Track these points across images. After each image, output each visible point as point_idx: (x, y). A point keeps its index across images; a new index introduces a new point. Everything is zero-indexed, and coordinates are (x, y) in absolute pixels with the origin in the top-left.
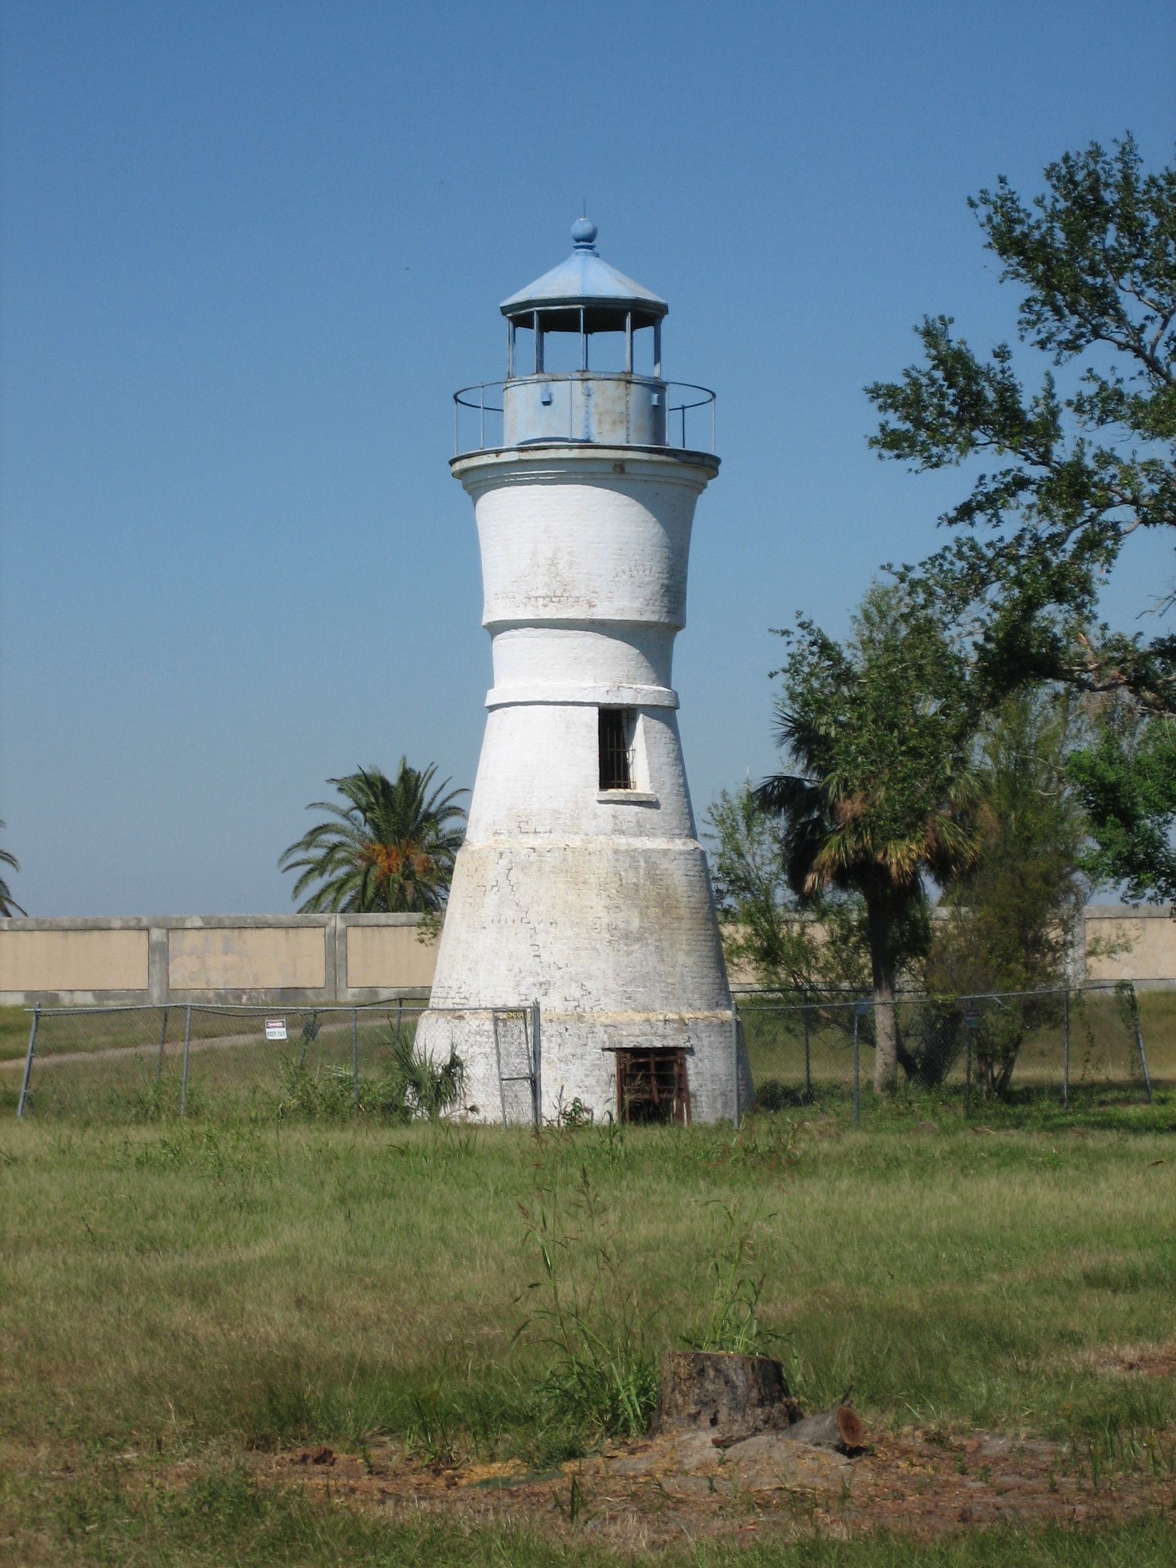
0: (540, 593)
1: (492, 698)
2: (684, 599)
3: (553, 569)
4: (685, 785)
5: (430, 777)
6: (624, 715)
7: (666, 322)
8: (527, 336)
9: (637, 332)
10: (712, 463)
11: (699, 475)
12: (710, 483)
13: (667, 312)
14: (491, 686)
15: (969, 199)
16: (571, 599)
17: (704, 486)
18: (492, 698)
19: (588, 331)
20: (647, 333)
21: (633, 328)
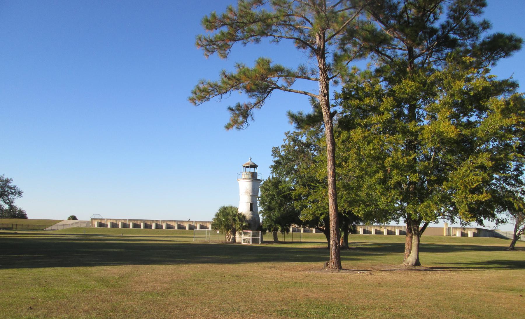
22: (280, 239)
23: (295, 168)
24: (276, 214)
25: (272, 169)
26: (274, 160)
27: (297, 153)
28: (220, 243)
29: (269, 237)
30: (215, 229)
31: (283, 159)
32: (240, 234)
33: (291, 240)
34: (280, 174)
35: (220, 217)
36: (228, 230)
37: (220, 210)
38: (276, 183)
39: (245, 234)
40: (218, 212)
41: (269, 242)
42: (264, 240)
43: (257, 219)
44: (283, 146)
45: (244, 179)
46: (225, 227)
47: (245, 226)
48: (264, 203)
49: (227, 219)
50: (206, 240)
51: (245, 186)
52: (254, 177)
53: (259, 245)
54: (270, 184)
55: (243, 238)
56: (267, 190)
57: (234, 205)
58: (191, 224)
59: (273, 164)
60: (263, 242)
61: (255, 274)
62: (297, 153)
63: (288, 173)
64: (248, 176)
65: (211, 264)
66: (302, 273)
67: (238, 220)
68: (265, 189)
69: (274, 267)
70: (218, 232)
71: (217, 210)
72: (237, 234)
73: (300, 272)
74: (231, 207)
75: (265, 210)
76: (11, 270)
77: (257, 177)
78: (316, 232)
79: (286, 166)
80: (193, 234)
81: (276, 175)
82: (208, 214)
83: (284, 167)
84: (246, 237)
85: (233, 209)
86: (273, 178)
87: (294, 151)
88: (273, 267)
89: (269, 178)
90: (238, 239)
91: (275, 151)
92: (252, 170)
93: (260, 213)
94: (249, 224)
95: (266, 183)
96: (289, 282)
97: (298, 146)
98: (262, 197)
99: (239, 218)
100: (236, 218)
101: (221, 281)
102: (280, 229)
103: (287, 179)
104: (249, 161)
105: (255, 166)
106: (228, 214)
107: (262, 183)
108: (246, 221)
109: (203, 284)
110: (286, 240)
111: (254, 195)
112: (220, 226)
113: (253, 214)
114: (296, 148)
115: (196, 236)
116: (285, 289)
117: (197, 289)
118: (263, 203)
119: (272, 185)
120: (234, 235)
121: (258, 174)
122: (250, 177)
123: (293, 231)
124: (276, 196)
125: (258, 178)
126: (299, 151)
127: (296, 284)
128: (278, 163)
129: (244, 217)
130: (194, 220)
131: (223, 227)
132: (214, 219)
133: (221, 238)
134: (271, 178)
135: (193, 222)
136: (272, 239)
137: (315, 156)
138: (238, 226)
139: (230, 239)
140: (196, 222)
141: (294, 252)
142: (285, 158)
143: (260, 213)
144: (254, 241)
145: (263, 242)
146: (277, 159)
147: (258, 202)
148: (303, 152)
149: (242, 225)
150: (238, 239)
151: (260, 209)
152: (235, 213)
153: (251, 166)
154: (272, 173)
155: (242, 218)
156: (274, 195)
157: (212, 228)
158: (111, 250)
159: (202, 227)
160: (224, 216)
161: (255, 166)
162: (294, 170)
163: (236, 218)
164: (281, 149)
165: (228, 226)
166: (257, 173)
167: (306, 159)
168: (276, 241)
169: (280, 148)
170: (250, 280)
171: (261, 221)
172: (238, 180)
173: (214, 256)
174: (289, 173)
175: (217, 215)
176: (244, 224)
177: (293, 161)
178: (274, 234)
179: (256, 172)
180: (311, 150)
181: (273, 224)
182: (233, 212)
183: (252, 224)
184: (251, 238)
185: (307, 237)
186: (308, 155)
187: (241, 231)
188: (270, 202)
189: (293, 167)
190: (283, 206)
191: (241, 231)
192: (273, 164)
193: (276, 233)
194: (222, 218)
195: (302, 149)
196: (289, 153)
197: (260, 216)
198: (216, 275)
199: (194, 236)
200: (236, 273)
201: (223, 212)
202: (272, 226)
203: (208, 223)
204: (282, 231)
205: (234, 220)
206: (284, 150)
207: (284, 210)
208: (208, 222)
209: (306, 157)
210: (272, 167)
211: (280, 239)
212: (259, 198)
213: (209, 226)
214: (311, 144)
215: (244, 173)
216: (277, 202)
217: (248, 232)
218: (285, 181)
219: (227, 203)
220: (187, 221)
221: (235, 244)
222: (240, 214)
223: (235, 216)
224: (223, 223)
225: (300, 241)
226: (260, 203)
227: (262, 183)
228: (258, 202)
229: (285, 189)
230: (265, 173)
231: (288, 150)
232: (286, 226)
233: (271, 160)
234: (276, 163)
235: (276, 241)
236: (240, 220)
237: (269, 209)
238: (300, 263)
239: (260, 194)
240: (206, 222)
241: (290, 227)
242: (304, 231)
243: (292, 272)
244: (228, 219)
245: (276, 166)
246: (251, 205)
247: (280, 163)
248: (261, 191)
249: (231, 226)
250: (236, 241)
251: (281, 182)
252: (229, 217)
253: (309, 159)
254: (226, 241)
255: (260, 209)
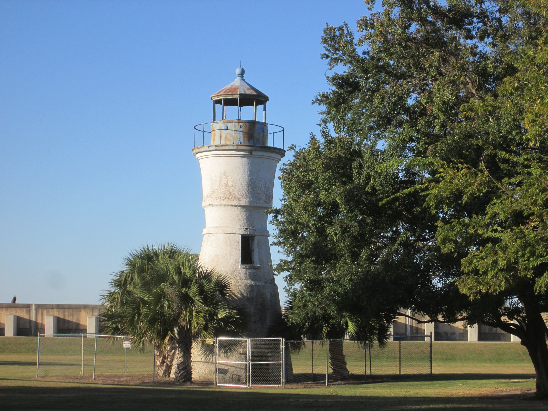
22: (355, 367)
23: (411, 102)
24: (343, 274)
26: (331, 74)
28: (134, 384)
29: (313, 358)
30: (116, 331)
32: (209, 349)
33: (393, 370)
34: (353, 127)
35: (130, 288)
36: (162, 335)
37: (132, 264)
38: (342, 162)
39: (227, 348)
40: (126, 269)
42: (297, 370)
44: (366, 24)
45: (218, 148)
46: (152, 322)
48: (294, 233)
49: (160, 297)
50: (81, 372)
51: (220, 172)
52: (254, 139)
53: (279, 388)
54: (318, 165)
56: (307, 186)
57: (182, 244)
58: (23, 314)
59: (330, 89)
63: (385, 121)
64: (235, 136)
67: (198, 301)
68: (301, 180)
70: (127, 344)
71: (119, 265)
72: (196, 351)
74: (172, 253)
75: (301, 257)
76: (39, 386)
77: (265, 138)
78: (480, 338)
80: (34, 351)
81: (338, 129)
82: (88, 280)
83: (371, 101)
84: (231, 361)
85: (180, 259)
86: (330, 142)
87: (409, 39)
91: (336, 41)
92: (248, 113)
93: (281, 268)
94: (240, 311)
97: (423, 21)
98: (288, 210)
99: (202, 291)
102: (351, 328)
104: (237, 82)
105: (257, 99)
106: (162, 277)
108: (230, 303)
110: (377, 371)
111: (256, 203)
113: (253, 277)
114: (414, 27)
115: (44, 358)
118: (290, 235)
122: (239, 137)
125: (269, 144)
126: (426, 40)
128: (346, 86)
129: (221, 286)
130: (33, 301)
132: (111, 295)
134: (321, 140)
135: (28, 307)
136: (324, 368)
137: (483, 56)
138: (197, 322)
139: (169, 368)
140: (39, 307)
143: (281, 268)
144: (261, 374)
146: (342, 69)
147: (272, 230)
148: (440, 43)
150: (200, 369)
151: (278, 255)
152: (187, 273)
153: (246, 100)
154: (325, 121)
155: (213, 290)
156: (335, 206)
157: (101, 329)
159: (64, 327)
160: (146, 286)
161: (257, 99)
162: (407, 110)
163: (193, 290)
164: (358, 35)
167: (450, 70)
168: (340, 374)
169: (353, 28)
171: (284, 299)
172: (195, 149)
174: (389, 122)
175: (121, 283)
176: (221, 314)
177: (403, 76)
178: (331, 350)
179: (260, 119)
180: (469, 37)
181: (332, 310)
182: (178, 271)
183: (251, 315)
184: (249, 363)
185: (450, 358)
186: (456, 53)
187: (210, 341)
188: (321, 232)
189: (402, 98)
191: (210, 341)
192: (330, 89)
193: (341, 344)
194: (138, 293)
195: (436, 30)
197: (280, 280)
199: (35, 358)
203: (83, 313)
205: (186, 300)
207: (371, 259)
208: (85, 307)
209: (452, 60)
210: (324, 99)
211: (355, 367)
212: (277, 212)
213: (90, 324)
214: (468, 14)
215: (217, 126)
216: (345, 230)
217: (236, 343)
218: (374, 153)
219: (157, 239)
220: (8, 307)
221: (188, 387)
222: (207, 277)
223: (186, 283)
224: (143, 310)
225: (425, 371)
226: (284, 234)
228: (272, 230)
230: (299, 124)
233: (321, 76)
234: (340, 86)
235: (340, 374)
236: (207, 299)
237: (321, 254)
240: (78, 308)
242: (439, 336)
244: (159, 295)
245: (342, 97)
246: (247, 243)
247: (356, 87)
249: (175, 320)
250: (195, 376)
251: (358, 154)
253: (463, 69)
254: (155, 375)
255: (278, 255)
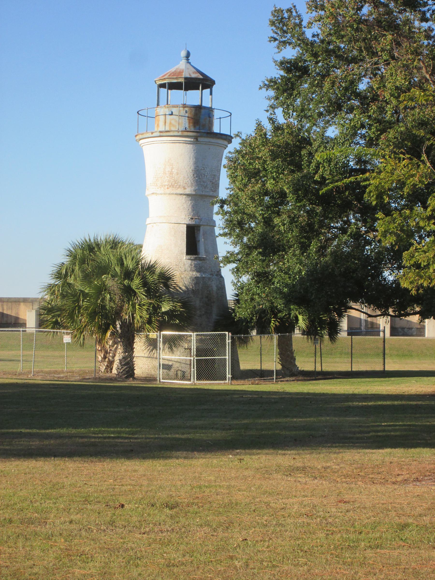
0: (166, 183)
1: (146, 223)
2: (219, 187)
3: (171, 175)
4: (6, 360)
5: (200, 144)
6: (196, 228)
7: (214, 87)
8: (163, 91)
9: (204, 91)
10: (230, 138)
11: (226, 143)
12: (229, 145)
13: (215, 84)
14: (148, 217)
15: (266, 111)
16: (177, 186)
17: (227, 146)
18: (146, 223)
19: (186, 89)
20: (207, 91)
21: (202, 90)
22: (304, 363)
23: (362, 86)
24: (293, 265)
25: (272, 93)
26: (279, 58)
27: (370, 27)
28: (75, 380)
29: (260, 353)
30: (56, 325)
31: (315, 55)
32: (152, 344)
33: (345, 367)
34: (303, 113)
35: (71, 280)
37: (73, 255)
38: (291, 150)
39: (172, 343)
40: (66, 260)
41: (262, 375)
42: (244, 366)
43: (214, 286)
45: (163, 134)
46: (92, 316)
47: (169, 313)
48: (240, 224)
49: (101, 290)
50: (20, 367)
51: (165, 159)
52: (200, 123)
54: (264, 153)
55: (161, 360)
56: (253, 175)
57: (125, 235)
59: (278, 73)
60: (239, 375)
61: (239, 496)
62: (370, 27)
63: (336, 107)
65: (58, 461)
66: (419, 489)
68: (248, 170)
69: (303, 470)
70: (67, 339)
71: (58, 256)
72: (139, 346)
73: (410, 487)
74: (115, 244)
75: (248, 249)
77: (211, 123)
79: (327, 85)
81: (286, 114)
83: (320, 86)
85: (122, 251)
86: (277, 128)
87: (360, 21)
88: (298, 469)
89: (259, 127)
90: (144, 362)
91: (284, 24)
92: (193, 97)
93: (227, 260)
94: (185, 304)
95: (249, 149)
96: (375, 526)
98: (234, 200)
99: (145, 284)
100: (136, 283)
101: (112, 523)
102: (302, 322)
103: (332, 132)
104: (182, 65)
105: (203, 83)
106: (103, 269)
107: (235, 144)
108: (174, 296)
109: (49, 537)
110: (328, 367)
111: (202, 192)
112: (71, 316)
113: (198, 269)
116: (369, 553)
117: (28, 557)
118: (237, 226)
119: (274, 156)
120: (129, 347)
121: (217, 114)
122: (185, 123)
123: (352, 332)
124: (290, 197)
125: (216, 129)
126: (379, 22)
127: (407, 534)
128: (295, 70)
129: (166, 278)
131: (85, 320)
132: (51, 288)
133: (76, 360)
134: (268, 127)
136: (273, 364)
138: (141, 315)
139: (111, 363)
141: (366, 411)
142: (322, 51)
143: (227, 260)
144: (206, 369)
145: (239, 375)
146: (291, 53)
147: (219, 221)
148: (392, 26)
149: (156, 309)
151: (225, 246)
152: (129, 264)
154: (273, 107)
155: (157, 283)
156: (283, 195)
157: (41, 323)
158: (356, 404)
160: (87, 278)
161: (203, 83)
162: (358, 95)
163: (136, 283)
165: (105, 316)
166: (211, 110)
167: (403, 54)
168: (289, 370)
170: (222, 519)
171: (230, 292)
172: (138, 136)
173: (64, 431)
174: (339, 108)
175: (61, 275)
176: (165, 307)
177: (354, 60)
178: (280, 345)
179: (206, 103)
181: (279, 304)
182: (121, 262)
183: (198, 309)
184: (193, 358)
186: (410, 36)
187: (153, 335)
188: (268, 222)
190: (318, 234)
191: (153, 335)
192: (278, 73)
196: (338, 30)
197: (227, 272)
198: (86, 501)
200: (163, 495)
201: (83, 261)
202: (274, 311)
203: (22, 306)
204: (311, 332)
205: (129, 292)
206: (320, 19)
207: (322, 249)
208: (25, 300)
210: (271, 83)
211: (304, 363)
212: (223, 202)
213: (30, 318)
215: (162, 110)
219: (98, 229)
222: (151, 268)
223: (128, 274)
224: (84, 304)
225: (379, 368)
226: (230, 223)
227: (235, 144)
228: (219, 221)
229: (325, 171)
230: (246, 109)
231: (334, 16)
232: (327, 311)
233: (267, 60)
234: (288, 70)
235: (289, 370)
236: (151, 291)
238: (399, 452)
239: (225, 188)
241: (340, 315)
242: (394, 332)
243: (378, 487)
244: (100, 289)
245: (290, 82)
246: (192, 233)
247: (305, 71)
248: (233, 178)
252: (110, 282)
253: (417, 53)
254: (96, 371)
255: (225, 246)
